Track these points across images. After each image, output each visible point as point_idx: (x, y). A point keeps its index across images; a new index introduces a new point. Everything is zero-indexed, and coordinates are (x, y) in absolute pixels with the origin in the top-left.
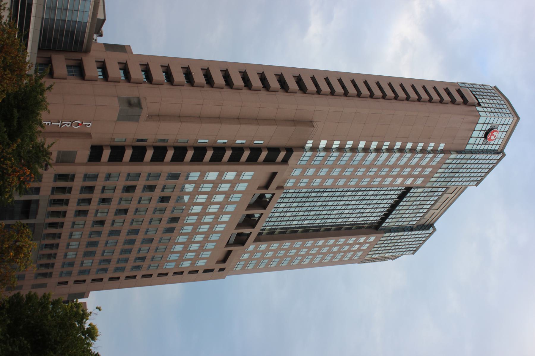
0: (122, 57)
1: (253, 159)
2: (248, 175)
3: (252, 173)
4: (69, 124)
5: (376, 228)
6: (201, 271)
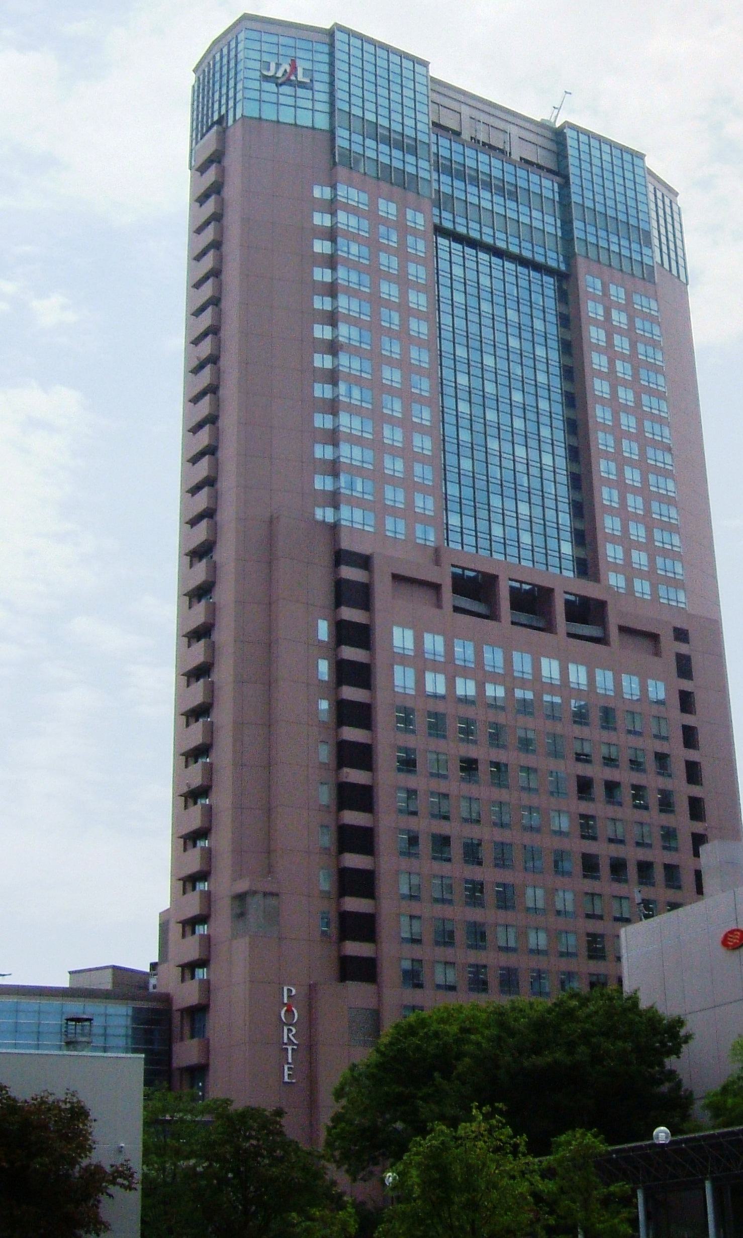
0: (176, 930)
1: (361, 635)
2: (402, 639)
3: (397, 632)
6: (687, 685)
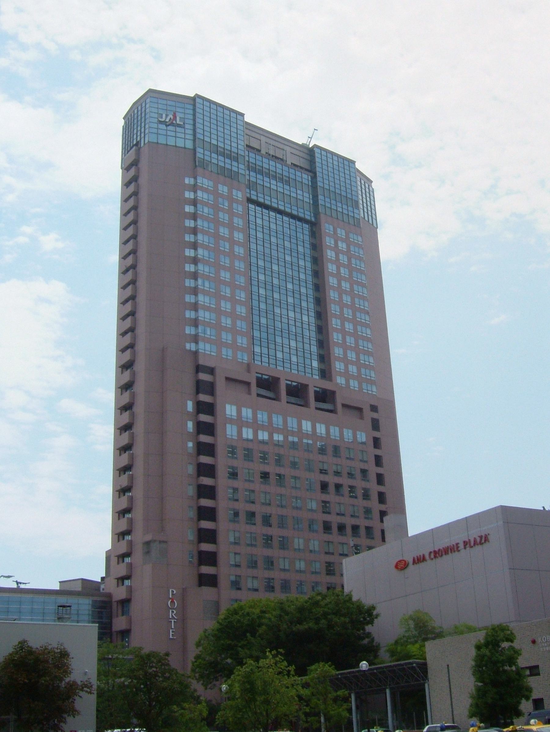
0: (114, 560)
2: (231, 410)
3: (228, 407)
4: (173, 591)
5: (314, 226)
